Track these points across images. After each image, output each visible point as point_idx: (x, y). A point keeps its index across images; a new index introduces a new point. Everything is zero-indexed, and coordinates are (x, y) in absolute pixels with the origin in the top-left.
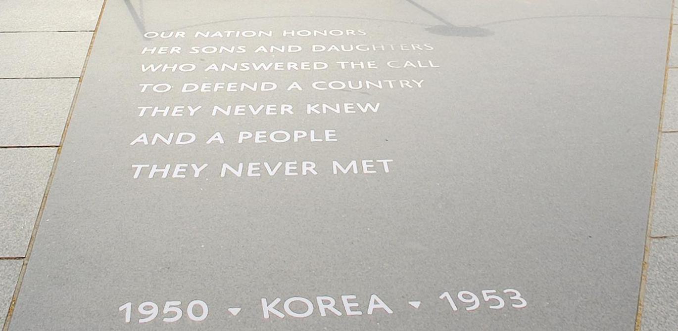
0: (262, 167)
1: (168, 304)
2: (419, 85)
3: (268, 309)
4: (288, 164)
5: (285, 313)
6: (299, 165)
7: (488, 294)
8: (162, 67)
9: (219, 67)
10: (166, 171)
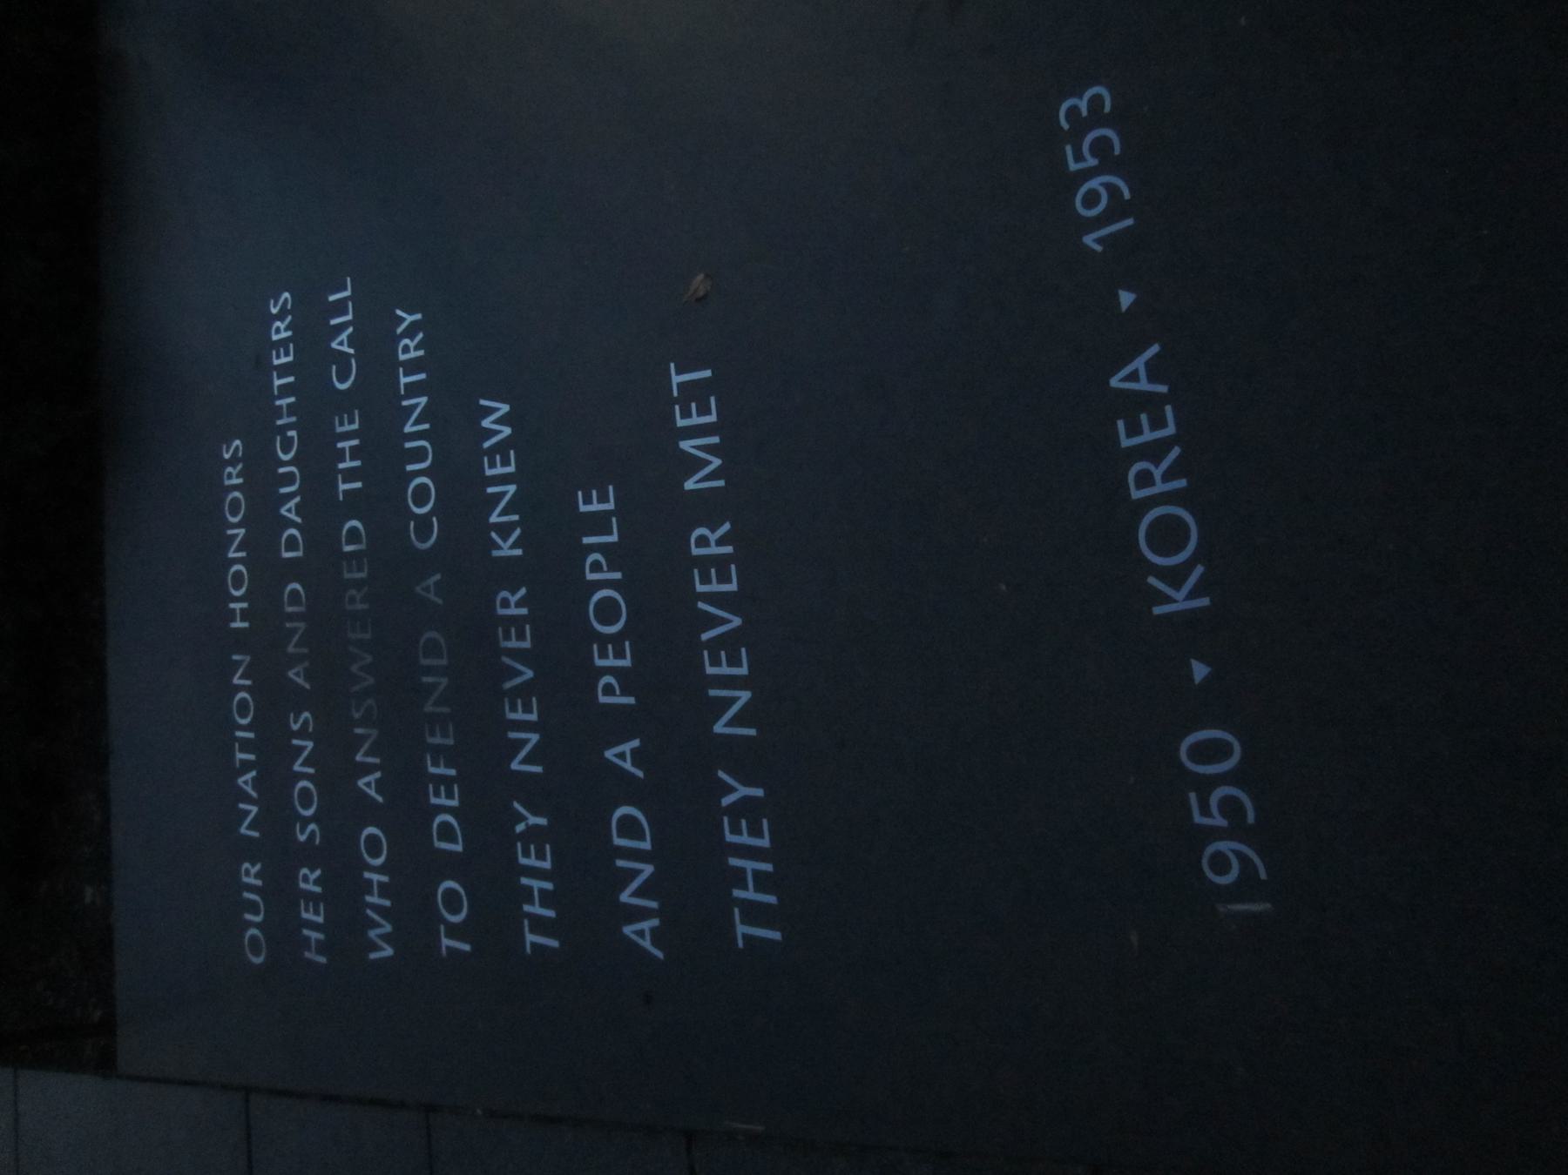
0: (715, 645)
1: (1198, 818)
2: (410, 318)
3: (1180, 601)
4: (700, 588)
5: (1189, 565)
6: (705, 563)
7: (1079, 157)
8: (376, 908)
9: (367, 769)
10: (315, 935)
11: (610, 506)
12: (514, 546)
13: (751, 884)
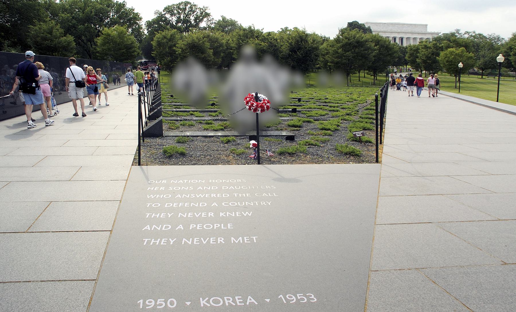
1: (159, 300)
3: (203, 302)
7: (300, 296)
9: (182, 196)
11: (229, 228)
12: (204, 304)
13: (154, 241)
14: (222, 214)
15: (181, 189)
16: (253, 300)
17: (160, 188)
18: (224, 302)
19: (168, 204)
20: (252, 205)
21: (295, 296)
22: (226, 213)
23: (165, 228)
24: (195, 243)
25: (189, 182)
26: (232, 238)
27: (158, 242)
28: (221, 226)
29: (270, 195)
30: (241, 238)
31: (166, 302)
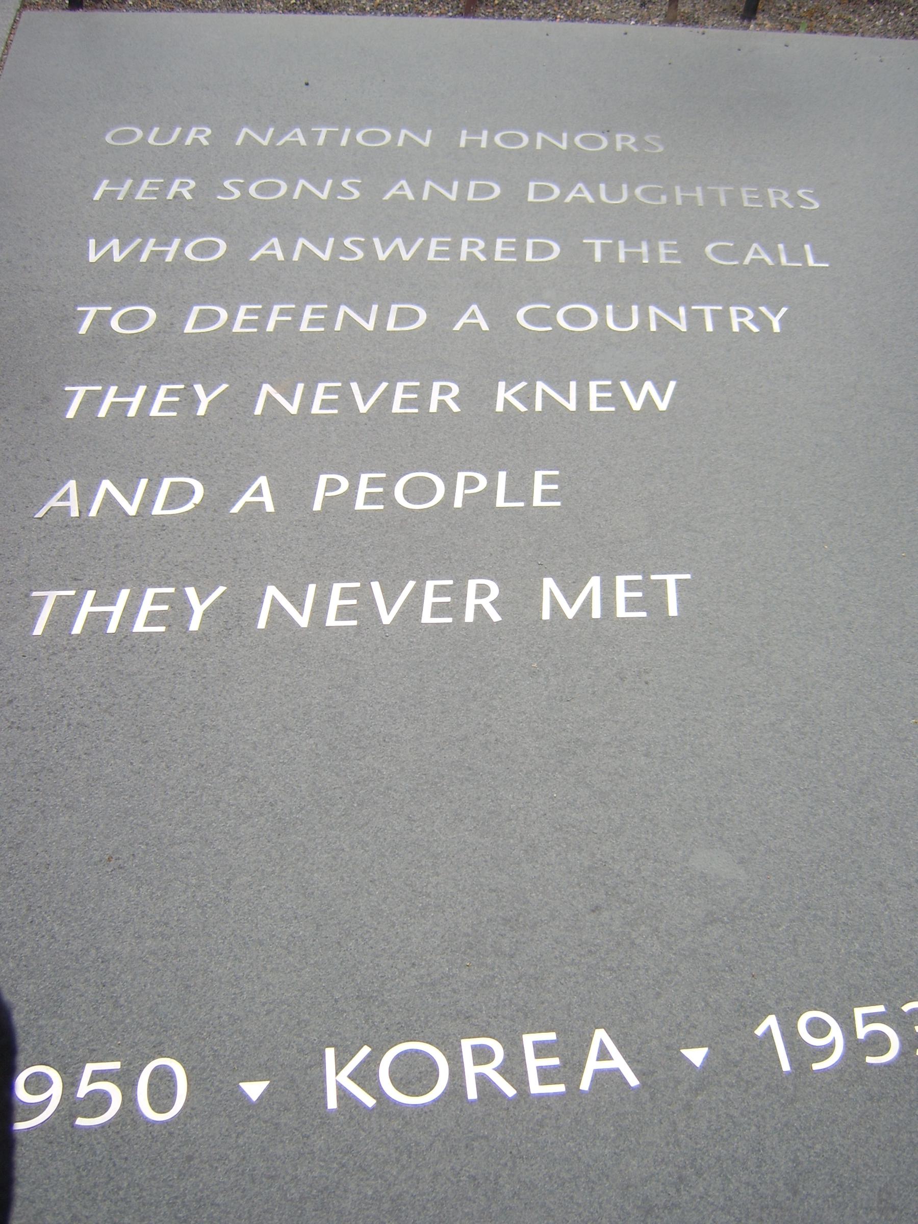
7: (869, 1019)
14: (509, 396)
15: (291, 191)
16: (618, 1062)
17: (166, 187)
18: (457, 1073)
19: (156, 595)
20: (683, 327)
21: (841, 1024)
22: (531, 388)
23: (146, 625)
24: (331, 621)
25: (344, 142)
26: (549, 584)
27: (136, 402)
28: (491, 490)
29: (784, 260)
30: (595, 583)
31: (127, 1081)
